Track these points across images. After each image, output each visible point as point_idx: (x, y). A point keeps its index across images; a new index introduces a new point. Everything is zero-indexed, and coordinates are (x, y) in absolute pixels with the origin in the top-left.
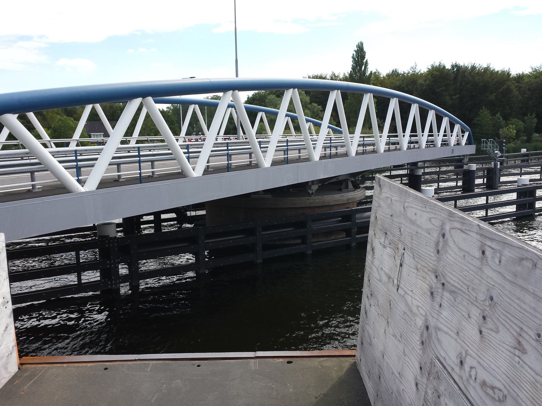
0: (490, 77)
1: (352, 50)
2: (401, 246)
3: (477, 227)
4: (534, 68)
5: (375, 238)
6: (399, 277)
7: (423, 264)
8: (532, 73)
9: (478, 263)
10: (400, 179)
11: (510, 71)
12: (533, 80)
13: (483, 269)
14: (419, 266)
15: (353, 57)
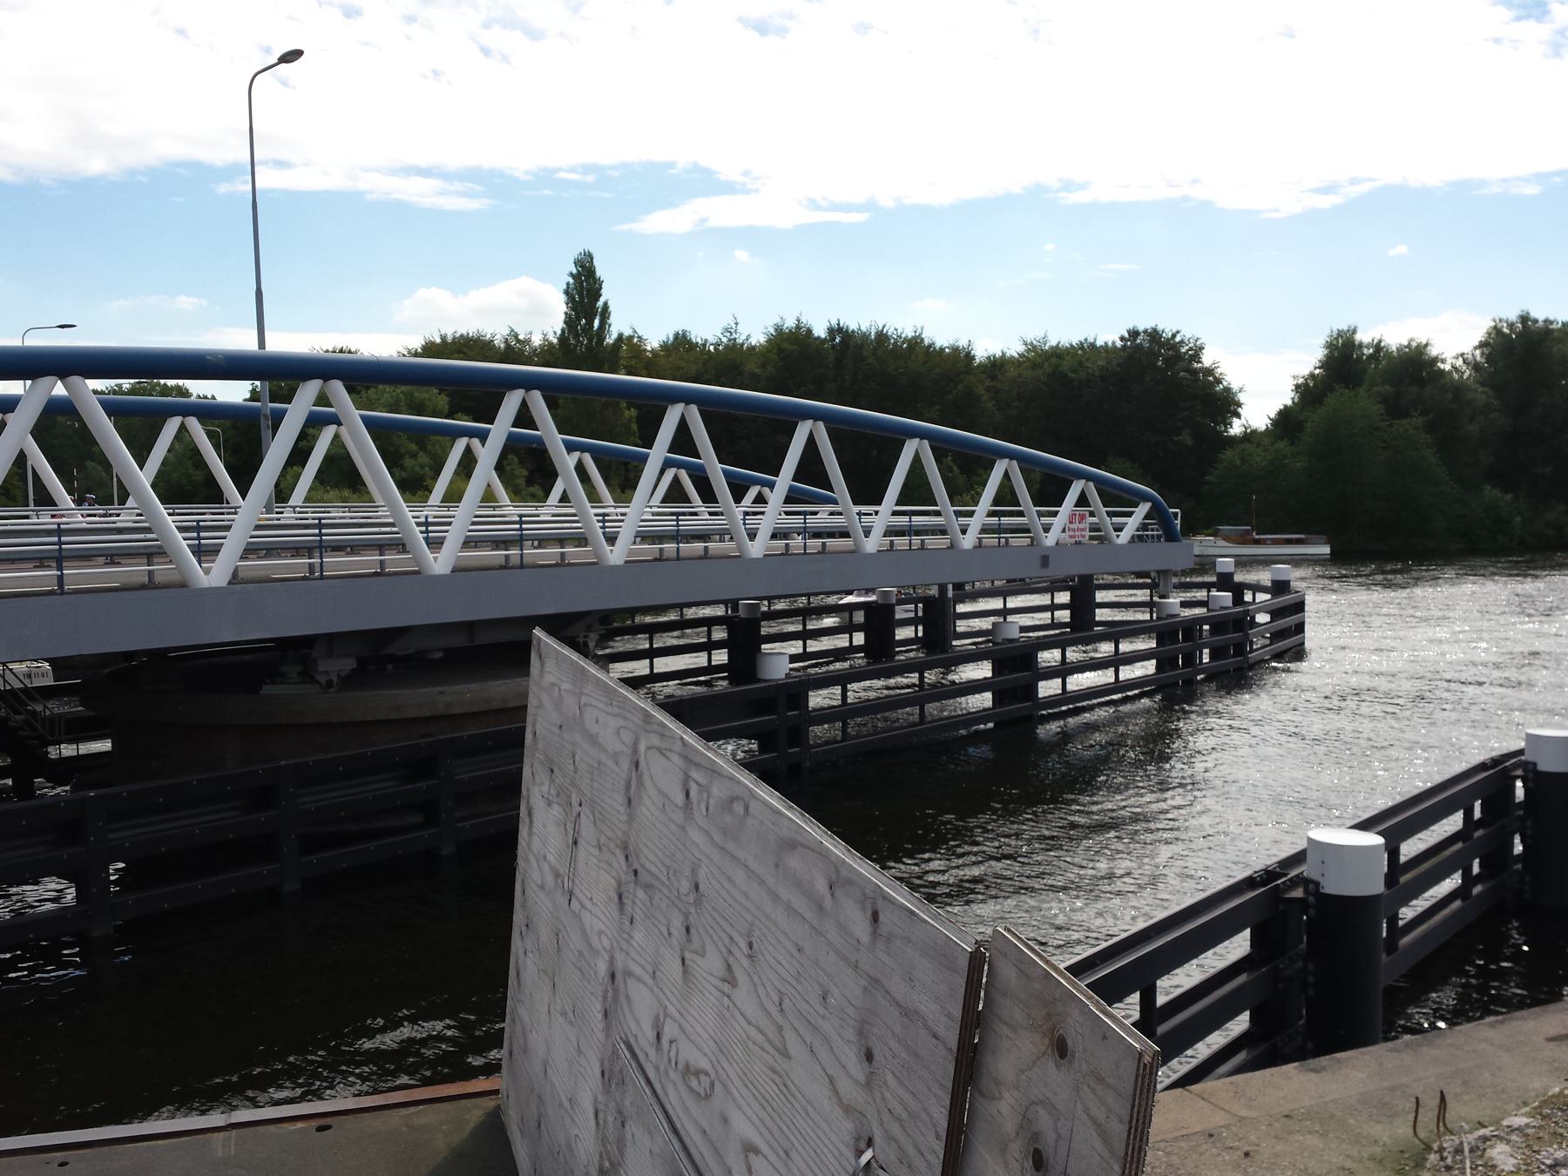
0: (924, 363)
1: (565, 270)
2: (575, 799)
3: (679, 743)
4: (1029, 341)
5: (534, 784)
6: (572, 870)
7: (610, 833)
8: (1025, 356)
9: (679, 817)
10: (706, 628)
11: (972, 349)
13: (687, 829)
14: (603, 840)
15: (567, 292)
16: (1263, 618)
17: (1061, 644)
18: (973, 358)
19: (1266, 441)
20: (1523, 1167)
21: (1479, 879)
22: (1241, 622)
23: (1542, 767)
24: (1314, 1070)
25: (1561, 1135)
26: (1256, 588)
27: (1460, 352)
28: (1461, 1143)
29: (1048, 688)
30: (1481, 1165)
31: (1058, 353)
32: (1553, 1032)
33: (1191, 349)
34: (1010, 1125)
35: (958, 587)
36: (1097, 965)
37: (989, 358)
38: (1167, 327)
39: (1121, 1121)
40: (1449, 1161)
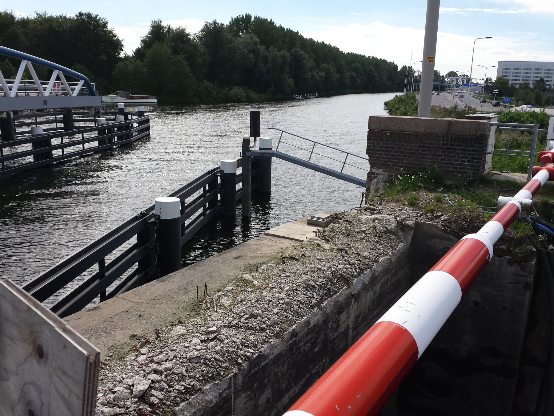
12: (39, 27)
16: (135, 125)
17: (61, 136)
18: (15, 18)
19: (133, 60)
20: (232, 304)
21: (208, 209)
22: (128, 127)
23: (225, 172)
24: (162, 281)
25: (242, 291)
26: (132, 114)
27: (195, 33)
28: (213, 299)
29: (57, 153)
30: (219, 305)
31: (51, 19)
32: (235, 256)
33: (103, 23)
34: (15, 395)
35: (15, 113)
36: (82, 255)
37: (21, 19)
38: (94, 13)
39: (78, 398)
40: (209, 306)
